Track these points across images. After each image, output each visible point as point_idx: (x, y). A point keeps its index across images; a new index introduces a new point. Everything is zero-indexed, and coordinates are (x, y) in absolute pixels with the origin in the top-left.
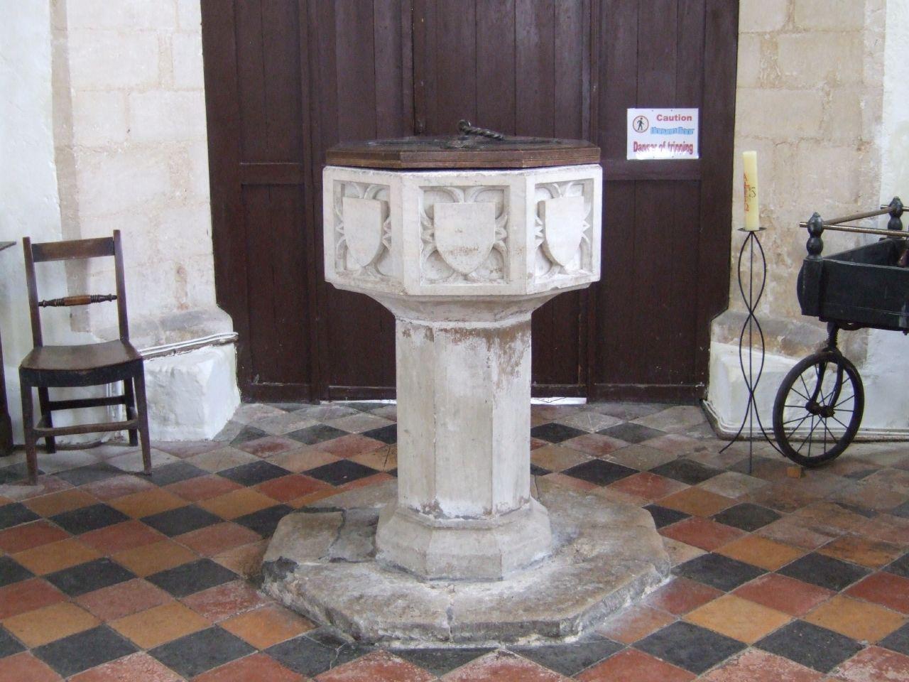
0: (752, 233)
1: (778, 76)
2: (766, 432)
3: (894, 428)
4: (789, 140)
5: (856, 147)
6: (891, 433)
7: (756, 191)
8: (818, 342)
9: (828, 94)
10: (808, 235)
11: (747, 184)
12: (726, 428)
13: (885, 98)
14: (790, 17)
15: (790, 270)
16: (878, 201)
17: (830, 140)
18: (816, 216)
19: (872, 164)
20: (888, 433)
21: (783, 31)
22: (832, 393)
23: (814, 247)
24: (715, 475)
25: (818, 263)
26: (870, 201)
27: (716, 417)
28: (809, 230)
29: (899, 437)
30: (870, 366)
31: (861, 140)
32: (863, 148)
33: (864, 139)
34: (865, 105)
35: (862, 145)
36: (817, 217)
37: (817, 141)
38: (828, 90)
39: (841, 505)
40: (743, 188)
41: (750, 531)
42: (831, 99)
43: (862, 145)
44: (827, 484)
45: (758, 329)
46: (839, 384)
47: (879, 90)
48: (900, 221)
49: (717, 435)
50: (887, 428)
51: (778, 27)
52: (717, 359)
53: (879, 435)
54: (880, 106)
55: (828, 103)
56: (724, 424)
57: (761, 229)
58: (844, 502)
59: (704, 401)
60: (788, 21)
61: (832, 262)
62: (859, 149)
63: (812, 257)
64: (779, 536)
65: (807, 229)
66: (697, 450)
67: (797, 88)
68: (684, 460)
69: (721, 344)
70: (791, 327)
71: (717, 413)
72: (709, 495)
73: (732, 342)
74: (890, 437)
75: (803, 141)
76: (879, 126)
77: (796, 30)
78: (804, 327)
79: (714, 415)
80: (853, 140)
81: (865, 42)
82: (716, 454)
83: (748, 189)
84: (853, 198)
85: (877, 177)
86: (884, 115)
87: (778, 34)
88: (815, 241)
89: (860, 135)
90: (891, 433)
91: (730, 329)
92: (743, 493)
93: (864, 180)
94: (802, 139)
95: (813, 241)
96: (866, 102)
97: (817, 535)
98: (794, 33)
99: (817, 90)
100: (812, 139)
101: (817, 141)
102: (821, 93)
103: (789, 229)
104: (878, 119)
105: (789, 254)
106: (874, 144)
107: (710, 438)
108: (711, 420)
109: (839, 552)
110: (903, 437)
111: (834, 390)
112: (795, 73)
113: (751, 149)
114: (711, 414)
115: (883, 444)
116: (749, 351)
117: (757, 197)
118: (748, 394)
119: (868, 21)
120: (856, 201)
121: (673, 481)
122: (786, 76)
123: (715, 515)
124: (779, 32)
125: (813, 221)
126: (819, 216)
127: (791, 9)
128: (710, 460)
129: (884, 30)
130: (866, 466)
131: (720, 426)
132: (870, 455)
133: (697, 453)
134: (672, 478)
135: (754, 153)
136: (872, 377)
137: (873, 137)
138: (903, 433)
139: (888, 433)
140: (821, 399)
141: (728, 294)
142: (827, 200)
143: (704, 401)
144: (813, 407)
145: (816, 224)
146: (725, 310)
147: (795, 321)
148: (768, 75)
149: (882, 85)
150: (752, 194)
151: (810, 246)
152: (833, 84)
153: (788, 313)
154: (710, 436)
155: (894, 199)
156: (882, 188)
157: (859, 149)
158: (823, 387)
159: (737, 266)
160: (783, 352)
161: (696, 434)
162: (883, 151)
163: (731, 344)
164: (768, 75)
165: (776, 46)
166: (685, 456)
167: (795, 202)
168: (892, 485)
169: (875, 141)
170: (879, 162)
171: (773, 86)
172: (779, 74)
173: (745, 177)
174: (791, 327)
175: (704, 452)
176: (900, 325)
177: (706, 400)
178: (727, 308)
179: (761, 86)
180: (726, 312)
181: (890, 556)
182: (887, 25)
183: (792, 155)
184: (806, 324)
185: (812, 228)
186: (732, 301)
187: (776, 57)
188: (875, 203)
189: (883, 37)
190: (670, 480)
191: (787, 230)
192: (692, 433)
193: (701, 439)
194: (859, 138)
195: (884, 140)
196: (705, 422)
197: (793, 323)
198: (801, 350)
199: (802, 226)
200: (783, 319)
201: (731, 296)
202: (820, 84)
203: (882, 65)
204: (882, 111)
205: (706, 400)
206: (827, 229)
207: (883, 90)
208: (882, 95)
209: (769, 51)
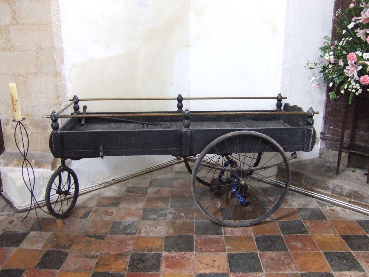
0: (20, 122)
1: (12, 45)
2: (38, 203)
3: (88, 187)
4: (22, 74)
5: (55, 75)
6: (87, 189)
7: (18, 102)
8: (51, 160)
9: (38, 53)
10: (51, 121)
11: (13, 99)
12: (19, 207)
13: (64, 53)
14: (14, 18)
15: (31, 131)
16: (67, 97)
17: (42, 73)
18: (54, 112)
19: (63, 82)
20: (86, 190)
21: (11, 24)
22: (67, 182)
23: (56, 127)
24: (25, 236)
25: (59, 134)
26: (64, 98)
27: (12, 202)
28: (52, 119)
29: (90, 190)
30: (74, 165)
31: (57, 72)
32: (58, 76)
33: (58, 72)
34: (57, 57)
35: (57, 74)
36: (54, 112)
37: (36, 74)
38: (38, 51)
39: (88, 236)
40: (11, 101)
41: (59, 269)
42: (40, 55)
43: (57, 74)
44: (78, 225)
45: (29, 164)
46: (69, 180)
47: (62, 50)
48: (78, 105)
49: (16, 211)
50: (84, 188)
51: (8, 23)
52: (5, 175)
53: (82, 191)
54: (63, 57)
55: (39, 56)
56: (17, 205)
57: (23, 119)
58: (89, 234)
59: (2, 192)
60: (13, 20)
61: (65, 132)
62: (56, 76)
63: (55, 132)
64: (73, 267)
65: (50, 119)
66: (10, 223)
67: (23, 51)
68: (6, 232)
69: (5, 167)
70: (36, 155)
71: (11, 199)
72: (29, 251)
73: (10, 165)
74: (87, 191)
75: (29, 74)
76: (63, 66)
77: (18, 24)
78: (42, 154)
79: (10, 200)
80: (53, 73)
81: (53, 29)
82: (20, 223)
83: (14, 102)
84: (57, 98)
85: (65, 88)
86: (65, 61)
87: (9, 26)
88: (55, 124)
89: (56, 70)
90: (87, 189)
91: (8, 160)
92: (43, 243)
93: (59, 90)
94: (28, 73)
95: (54, 124)
96: (57, 56)
97: (89, 260)
98: (17, 25)
99: (33, 51)
100: (34, 73)
101: (36, 74)
102: (35, 53)
103: (28, 114)
104: (62, 63)
105: (30, 124)
106: (62, 73)
107: (13, 213)
108: (9, 203)
109: (104, 267)
110: (93, 189)
111: (68, 180)
112: (20, 44)
113: (12, 82)
114: (8, 199)
115: (85, 195)
116: (21, 169)
117: (19, 104)
118: (31, 194)
119: (53, 20)
120: (58, 99)
121: (7, 248)
122: (16, 45)
123: (37, 264)
124: (9, 25)
125: (53, 115)
126: (55, 112)
127: (14, 14)
128: (20, 229)
129: (60, 24)
130: (86, 209)
131: (17, 208)
132: (84, 202)
133: (11, 225)
134: (5, 246)
135: (14, 84)
136: (75, 169)
137: (62, 71)
138: (91, 188)
139: (86, 190)
140: (63, 187)
141: (4, 144)
142: (44, 99)
143: (2, 192)
144: (59, 192)
145: (54, 116)
146: (4, 151)
147: (38, 152)
148: (7, 45)
149: (62, 48)
150: (17, 104)
151: (54, 126)
152: (40, 48)
153: (34, 149)
154: (13, 212)
155: (74, 96)
156: (68, 92)
157: (56, 76)
158: (63, 181)
159: (14, 136)
160: (36, 166)
161: (5, 213)
162: (66, 76)
163: (11, 167)
164: (7, 45)
165: (8, 31)
166: (6, 229)
167: (29, 101)
168: (101, 217)
169: (63, 72)
170: (65, 81)
171: (10, 50)
172: (12, 44)
173: (12, 96)
174: (36, 155)
175: (14, 223)
176: (101, 155)
177: (3, 192)
178: (4, 150)
179: (4, 50)
180: (4, 152)
181: (125, 260)
182: (61, 22)
183: (25, 81)
184: (43, 153)
185: (53, 118)
186: (6, 147)
187: (9, 37)
188: (66, 98)
189: (60, 27)
190: (4, 248)
191: (27, 114)
192: (3, 213)
193: (9, 215)
194: (56, 71)
195: (66, 72)
196: (7, 204)
197: (37, 153)
198: (44, 164)
199: (47, 117)
200: (32, 152)
201: (5, 145)
202: (34, 49)
203: (61, 39)
204: (64, 59)
205: (3, 192)
206: (59, 117)
207: (63, 50)
208: (63, 52)
209: (5, 34)
